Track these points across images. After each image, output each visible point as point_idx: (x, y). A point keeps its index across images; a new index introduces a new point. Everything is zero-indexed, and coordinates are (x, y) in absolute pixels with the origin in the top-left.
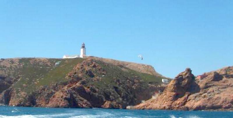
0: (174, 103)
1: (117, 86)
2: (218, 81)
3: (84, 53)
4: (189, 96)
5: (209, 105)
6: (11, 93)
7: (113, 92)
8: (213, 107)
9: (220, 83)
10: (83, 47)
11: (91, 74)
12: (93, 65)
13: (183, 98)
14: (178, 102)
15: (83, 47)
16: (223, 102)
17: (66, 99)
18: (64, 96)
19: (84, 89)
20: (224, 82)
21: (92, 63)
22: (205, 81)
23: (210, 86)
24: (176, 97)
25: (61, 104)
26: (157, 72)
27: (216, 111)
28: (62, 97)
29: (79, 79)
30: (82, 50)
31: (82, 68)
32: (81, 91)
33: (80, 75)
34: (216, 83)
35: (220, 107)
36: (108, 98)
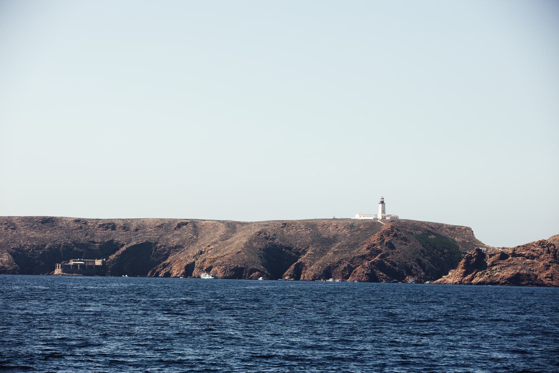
0: (463, 280)
1: (421, 258)
2: (504, 260)
3: (383, 211)
4: (476, 273)
5: (488, 281)
6: (302, 267)
7: (416, 266)
8: (492, 283)
9: (506, 262)
10: (382, 202)
11: (391, 246)
12: (394, 233)
13: (471, 275)
14: (466, 278)
15: (382, 202)
16: (501, 279)
17: (366, 274)
18: (366, 272)
19: (384, 263)
20: (509, 261)
21: (393, 231)
22: (492, 259)
23: (496, 265)
24: (465, 274)
25: (363, 279)
26: (477, 238)
27: (494, 286)
28: (363, 273)
29: (379, 252)
30: (381, 205)
31: (381, 238)
32: (380, 265)
33: (379, 247)
34: (501, 262)
35: (498, 283)
36: (410, 274)
